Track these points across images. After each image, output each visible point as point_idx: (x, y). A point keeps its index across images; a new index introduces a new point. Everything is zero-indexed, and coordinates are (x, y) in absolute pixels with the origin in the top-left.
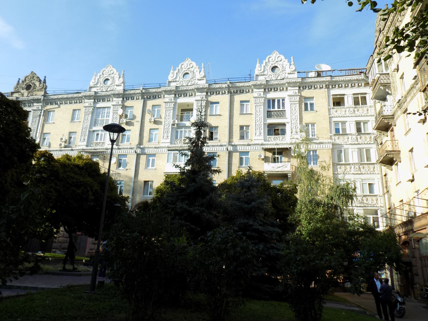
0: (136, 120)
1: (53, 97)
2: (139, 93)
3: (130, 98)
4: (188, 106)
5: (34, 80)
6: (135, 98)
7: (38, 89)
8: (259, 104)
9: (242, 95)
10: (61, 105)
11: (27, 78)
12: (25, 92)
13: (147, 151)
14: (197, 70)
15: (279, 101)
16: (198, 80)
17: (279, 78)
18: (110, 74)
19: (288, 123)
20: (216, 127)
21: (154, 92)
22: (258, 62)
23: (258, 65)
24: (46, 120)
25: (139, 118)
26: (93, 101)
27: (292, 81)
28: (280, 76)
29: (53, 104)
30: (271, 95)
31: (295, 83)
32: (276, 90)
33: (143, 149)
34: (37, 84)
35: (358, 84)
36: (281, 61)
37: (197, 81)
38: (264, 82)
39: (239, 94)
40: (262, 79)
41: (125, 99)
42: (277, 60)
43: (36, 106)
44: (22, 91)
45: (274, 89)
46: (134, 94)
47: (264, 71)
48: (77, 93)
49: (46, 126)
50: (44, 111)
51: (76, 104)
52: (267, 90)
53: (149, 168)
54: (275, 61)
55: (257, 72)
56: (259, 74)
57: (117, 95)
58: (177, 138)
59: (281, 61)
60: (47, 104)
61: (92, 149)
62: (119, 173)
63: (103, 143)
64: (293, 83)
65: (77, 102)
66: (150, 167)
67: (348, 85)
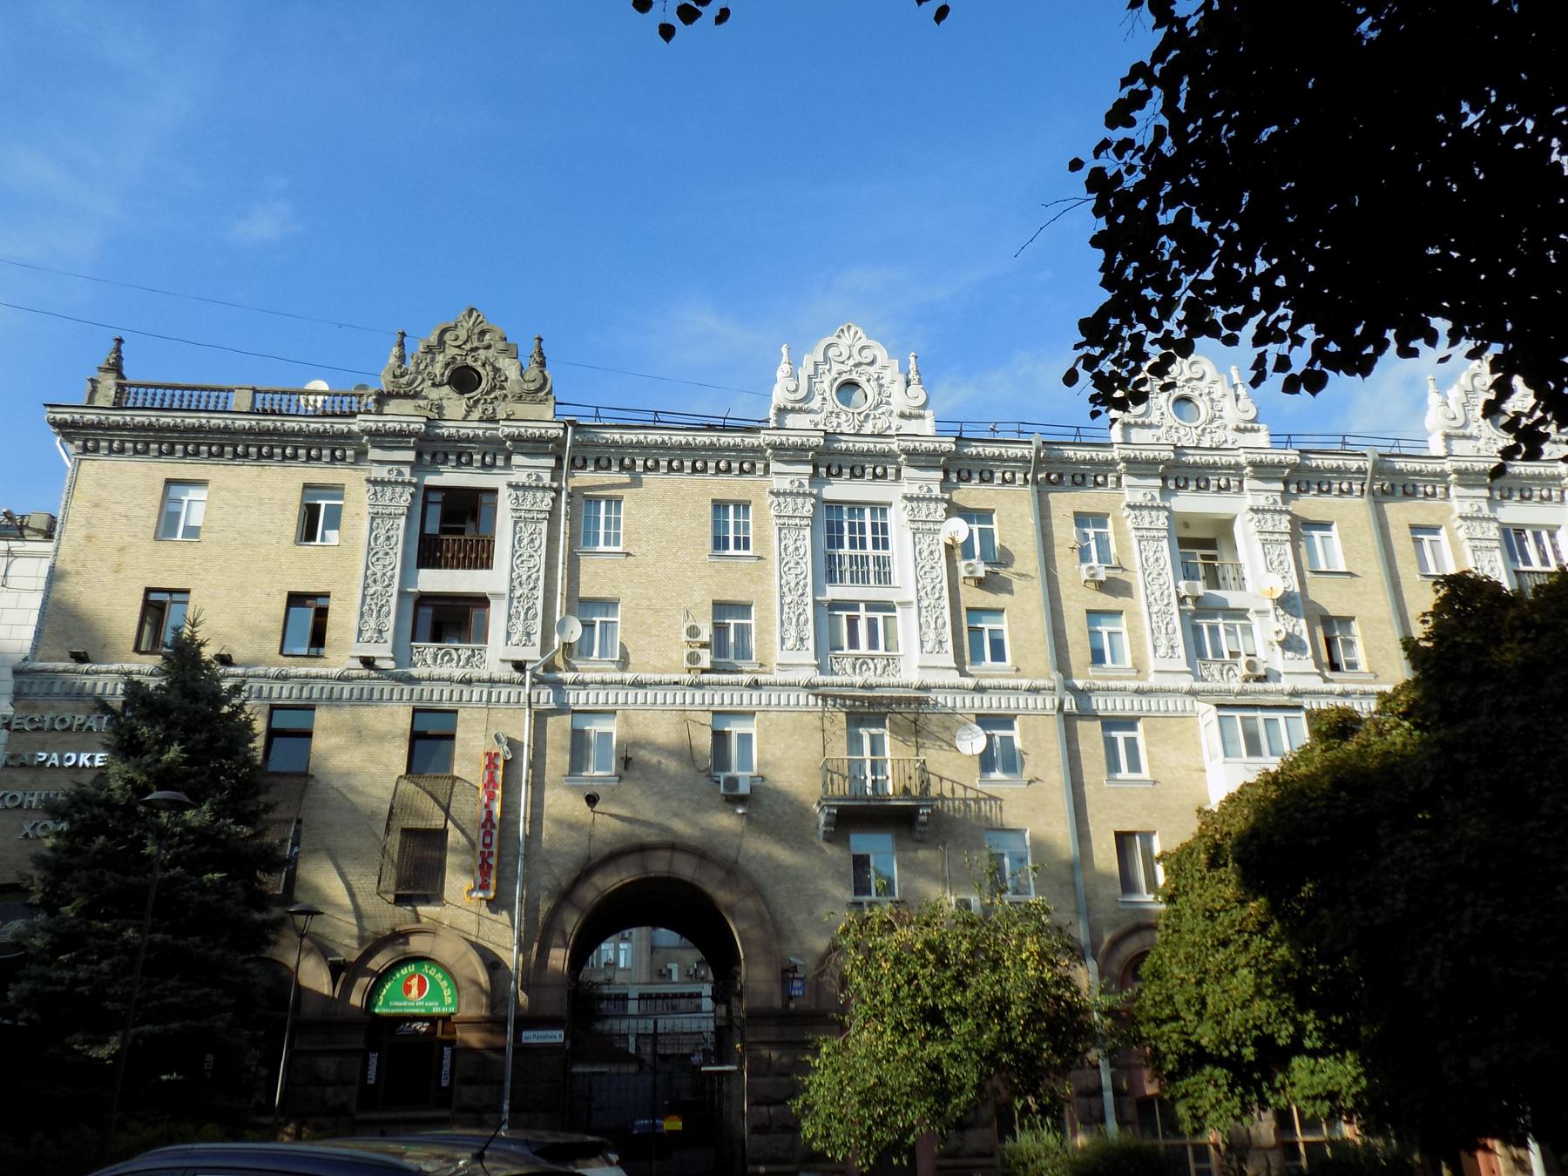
0: (1017, 566)
1: (615, 435)
2: (1023, 459)
3: (846, 471)
4: (1186, 525)
5: (488, 347)
6: (998, 475)
7: (517, 390)
9: (1410, 504)
10: (647, 478)
11: (448, 337)
12: (455, 405)
13: (1100, 704)
14: (892, 375)
15: (1537, 536)
17: (868, 429)
18: (477, 349)
19: (499, 596)
20: (1346, 621)
21: (1084, 462)
23: (783, 369)
24: (583, 537)
25: (1027, 558)
27: (792, 439)
28: (871, 422)
29: (608, 467)
30: (840, 490)
32: (856, 474)
33: (1082, 694)
34: (510, 369)
35: (670, 463)
36: (872, 363)
38: (817, 440)
39: (1399, 500)
40: (802, 429)
41: (954, 477)
42: (857, 359)
43: (524, 469)
44: (434, 394)
45: (852, 469)
47: (1465, 425)
48: (711, 428)
49: (587, 566)
50: (570, 496)
51: (724, 478)
52: (823, 470)
53: (1119, 776)
54: (851, 362)
56: (789, 406)
58: (1201, 654)
59: (872, 363)
61: (852, 686)
62: (991, 798)
63: (890, 660)
64: (1272, 465)
65: (729, 470)
66: (1125, 773)
67: (753, 465)
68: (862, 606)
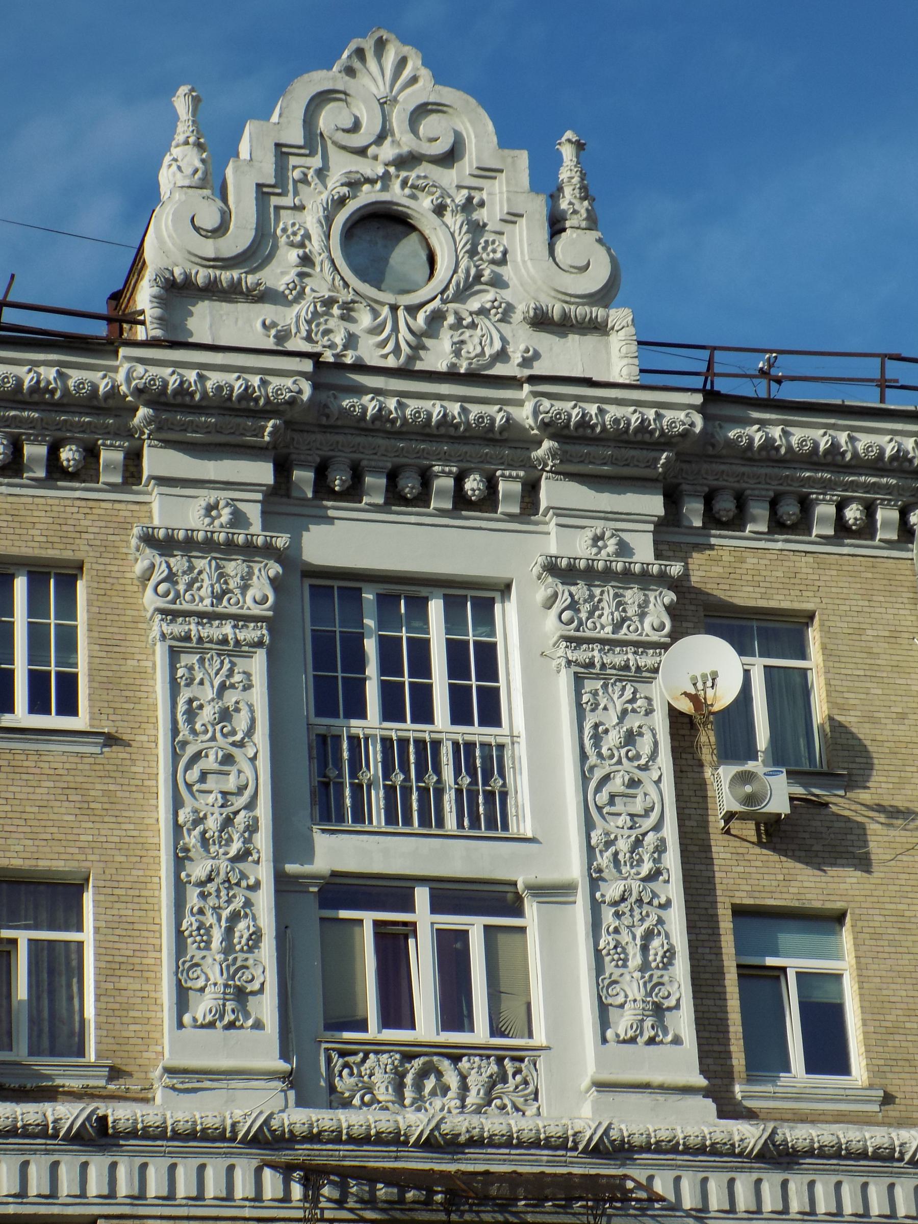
3: (375, 482)
8: (214, 631)
16: (541, 321)
17: (438, 356)
19: (554, 892)
22: (184, 130)
26: (262, 472)
27: (215, 379)
31: (643, 440)
36: (450, 158)
37: (522, 339)
38: (291, 383)
41: (694, 513)
42: (405, 142)
46: (832, 461)
54: (387, 151)
55: (167, 244)
56: (201, 276)
57: (601, 454)
59: (450, 158)
60: (339, 487)
61: (396, 1139)
64: (621, 438)
68: (422, 895)
